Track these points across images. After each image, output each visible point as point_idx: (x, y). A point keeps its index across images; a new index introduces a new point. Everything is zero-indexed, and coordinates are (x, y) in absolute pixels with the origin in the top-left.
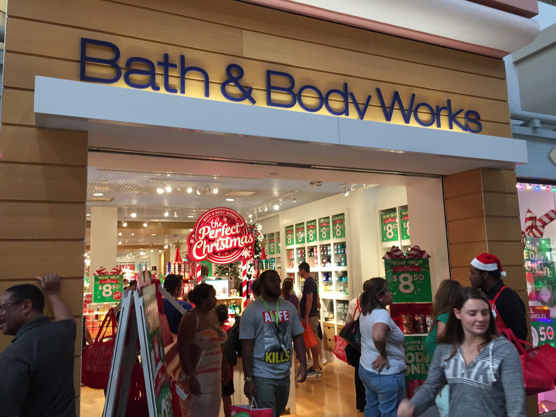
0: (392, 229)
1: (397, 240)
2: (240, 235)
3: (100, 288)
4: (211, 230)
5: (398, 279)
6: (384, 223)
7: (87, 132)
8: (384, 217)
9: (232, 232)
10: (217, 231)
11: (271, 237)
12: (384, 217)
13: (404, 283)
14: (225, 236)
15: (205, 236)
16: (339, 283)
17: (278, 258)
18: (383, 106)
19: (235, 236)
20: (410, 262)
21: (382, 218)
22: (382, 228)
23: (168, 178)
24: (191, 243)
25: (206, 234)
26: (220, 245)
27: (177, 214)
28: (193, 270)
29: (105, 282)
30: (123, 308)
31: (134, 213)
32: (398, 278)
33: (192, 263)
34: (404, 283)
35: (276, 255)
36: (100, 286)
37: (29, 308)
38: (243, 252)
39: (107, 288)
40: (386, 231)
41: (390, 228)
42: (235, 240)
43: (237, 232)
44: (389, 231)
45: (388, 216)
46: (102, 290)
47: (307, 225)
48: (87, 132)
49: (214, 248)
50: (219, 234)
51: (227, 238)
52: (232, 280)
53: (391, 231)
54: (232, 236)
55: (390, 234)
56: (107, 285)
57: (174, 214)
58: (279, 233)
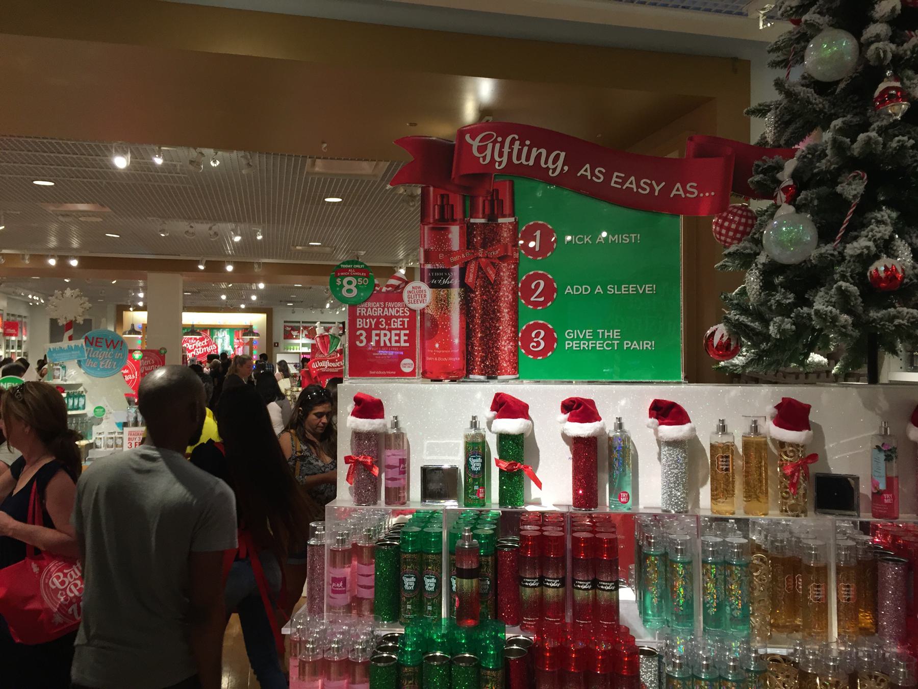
2: (208, 346)
3: (339, 283)
4: (145, 370)
5: (342, 283)
7: (750, 61)
9: (202, 345)
10: (193, 345)
13: (347, 287)
14: (199, 347)
16: (87, 436)
18: (107, 345)
19: (205, 346)
23: (386, 651)
26: (196, 352)
29: (345, 274)
30: (109, 433)
32: (342, 281)
33: (468, 232)
36: (338, 280)
37: (875, 125)
42: (205, 348)
43: (206, 344)
46: (342, 286)
48: (750, 61)
49: (193, 355)
50: (195, 347)
51: (200, 349)
54: (203, 347)
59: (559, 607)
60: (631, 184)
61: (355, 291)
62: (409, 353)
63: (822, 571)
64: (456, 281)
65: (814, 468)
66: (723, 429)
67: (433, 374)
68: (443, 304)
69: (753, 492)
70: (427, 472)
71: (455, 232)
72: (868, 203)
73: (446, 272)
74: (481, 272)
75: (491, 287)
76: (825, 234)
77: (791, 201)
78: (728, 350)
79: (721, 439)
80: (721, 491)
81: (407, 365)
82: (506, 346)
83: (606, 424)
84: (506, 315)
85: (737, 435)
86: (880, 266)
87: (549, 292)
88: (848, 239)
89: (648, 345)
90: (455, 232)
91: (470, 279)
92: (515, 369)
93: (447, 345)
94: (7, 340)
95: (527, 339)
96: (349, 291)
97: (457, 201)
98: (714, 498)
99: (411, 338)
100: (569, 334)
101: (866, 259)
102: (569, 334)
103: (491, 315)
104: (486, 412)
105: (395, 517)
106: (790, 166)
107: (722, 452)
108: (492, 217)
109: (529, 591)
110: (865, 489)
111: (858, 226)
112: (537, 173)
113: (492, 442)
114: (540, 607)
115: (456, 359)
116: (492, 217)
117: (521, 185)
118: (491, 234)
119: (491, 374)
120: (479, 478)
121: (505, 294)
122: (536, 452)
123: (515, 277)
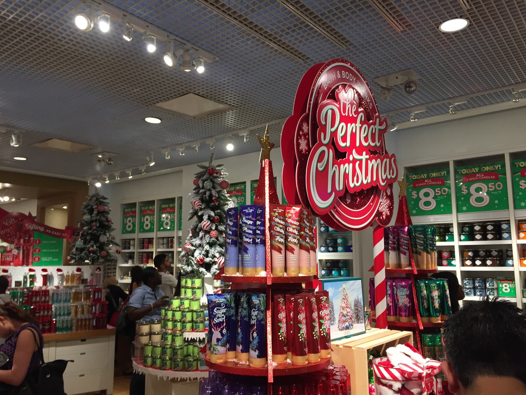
0: (131, 222)
1: (153, 231)
6: (143, 215)
8: (143, 208)
11: (144, 206)
12: (143, 208)
13: (505, 288)
15: (331, 133)
17: (159, 238)
20: (484, 169)
21: (124, 211)
22: (123, 221)
24: (300, 148)
25: (333, 129)
27: (18, 142)
28: (26, 252)
31: (74, 25)
33: (24, 240)
34: (505, 288)
35: (156, 235)
38: (380, 201)
39: (427, 195)
40: (144, 222)
41: (147, 220)
44: (146, 223)
45: (147, 208)
46: (502, 288)
47: (251, 186)
52: (100, 272)
53: (148, 223)
55: (147, 225)
56: (476, 185)
57: (10, 140)
58: (181, 198)
59: (39, 302)
60: (55, 233)
61: (509, 290)
62: (12, 262)
63: (82, 293)
64: (22, 249)
65: (82, 278)
66: (68, 272)
67: (16, 265)
68: (19, 253)
69: (72, 281)
70: (16, 282)
71: (22, 241)
72: (91, 239)
73: (20, 247)
74: (27, 247)
75: (28, 250)
76: (85, 243)
77: (81, 238)
78: (70, 260)
79: (67, 274)
80: (67, 282)
81: (12, 264)
82: (30, 260)
83: (49, 273)
84: (31, 255)
85: (70, 274)
86: (91, 249)
87: (39, 251)
88: (88, 244)
89: (57, 260)
90: (22, 241)
91: (24, 248)
92: (32, 264)
93: (19, 260)
94: (164, 328)
95: (35, 259)
96: (506, 290)
97: (22, 234)
98: (66, 282)
99: (13, 259)
100: (43, 258)
101: (89, 248)
102: (43, 258)
103: (28, 255)
104: (27, 271)
105: (274, 371)
106: (81, 233)
107: (68, 276)
108: (29, 238)
109: (34, 299)
110: (89, 280)
111: (89, 242)
112: (38, 231)
113: (28, 277)
114: (36, 302)
115: (21, 262)
116: (29, 238)
117: (35, 233)
118: (29, 240)
119: (27, 265)
120: (25, 282)
121: (31, 251)
122: (36, 278)
123: (33, 248)
